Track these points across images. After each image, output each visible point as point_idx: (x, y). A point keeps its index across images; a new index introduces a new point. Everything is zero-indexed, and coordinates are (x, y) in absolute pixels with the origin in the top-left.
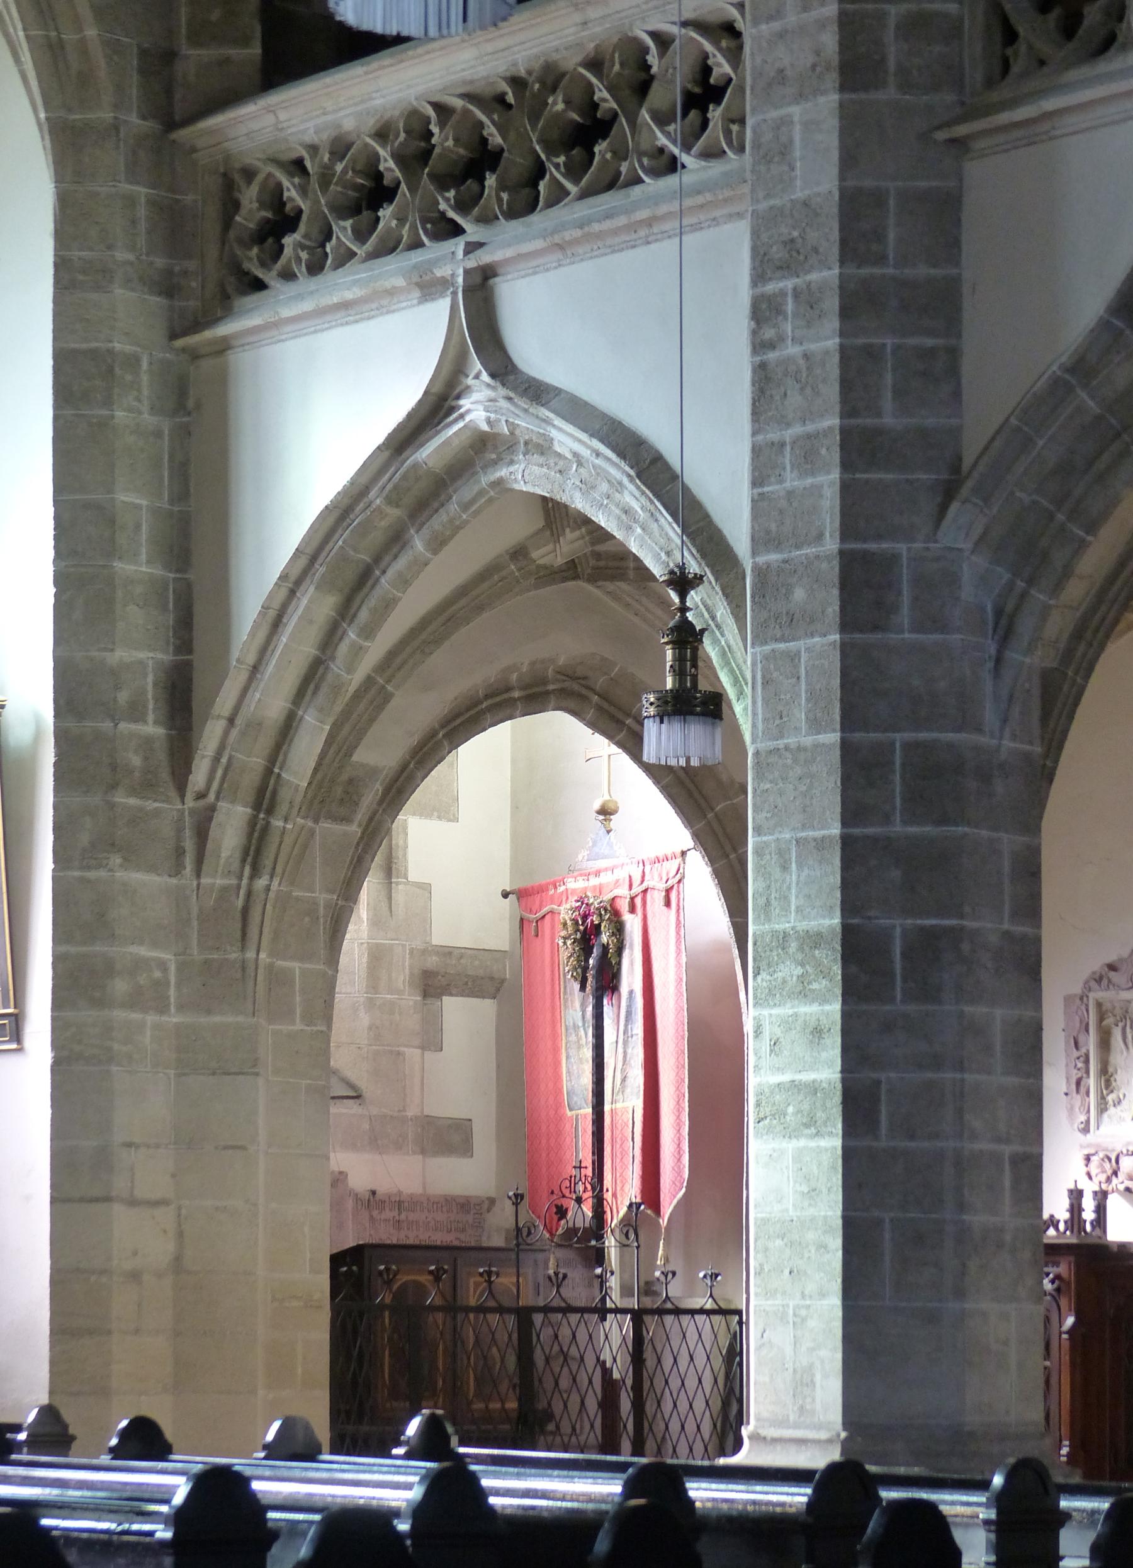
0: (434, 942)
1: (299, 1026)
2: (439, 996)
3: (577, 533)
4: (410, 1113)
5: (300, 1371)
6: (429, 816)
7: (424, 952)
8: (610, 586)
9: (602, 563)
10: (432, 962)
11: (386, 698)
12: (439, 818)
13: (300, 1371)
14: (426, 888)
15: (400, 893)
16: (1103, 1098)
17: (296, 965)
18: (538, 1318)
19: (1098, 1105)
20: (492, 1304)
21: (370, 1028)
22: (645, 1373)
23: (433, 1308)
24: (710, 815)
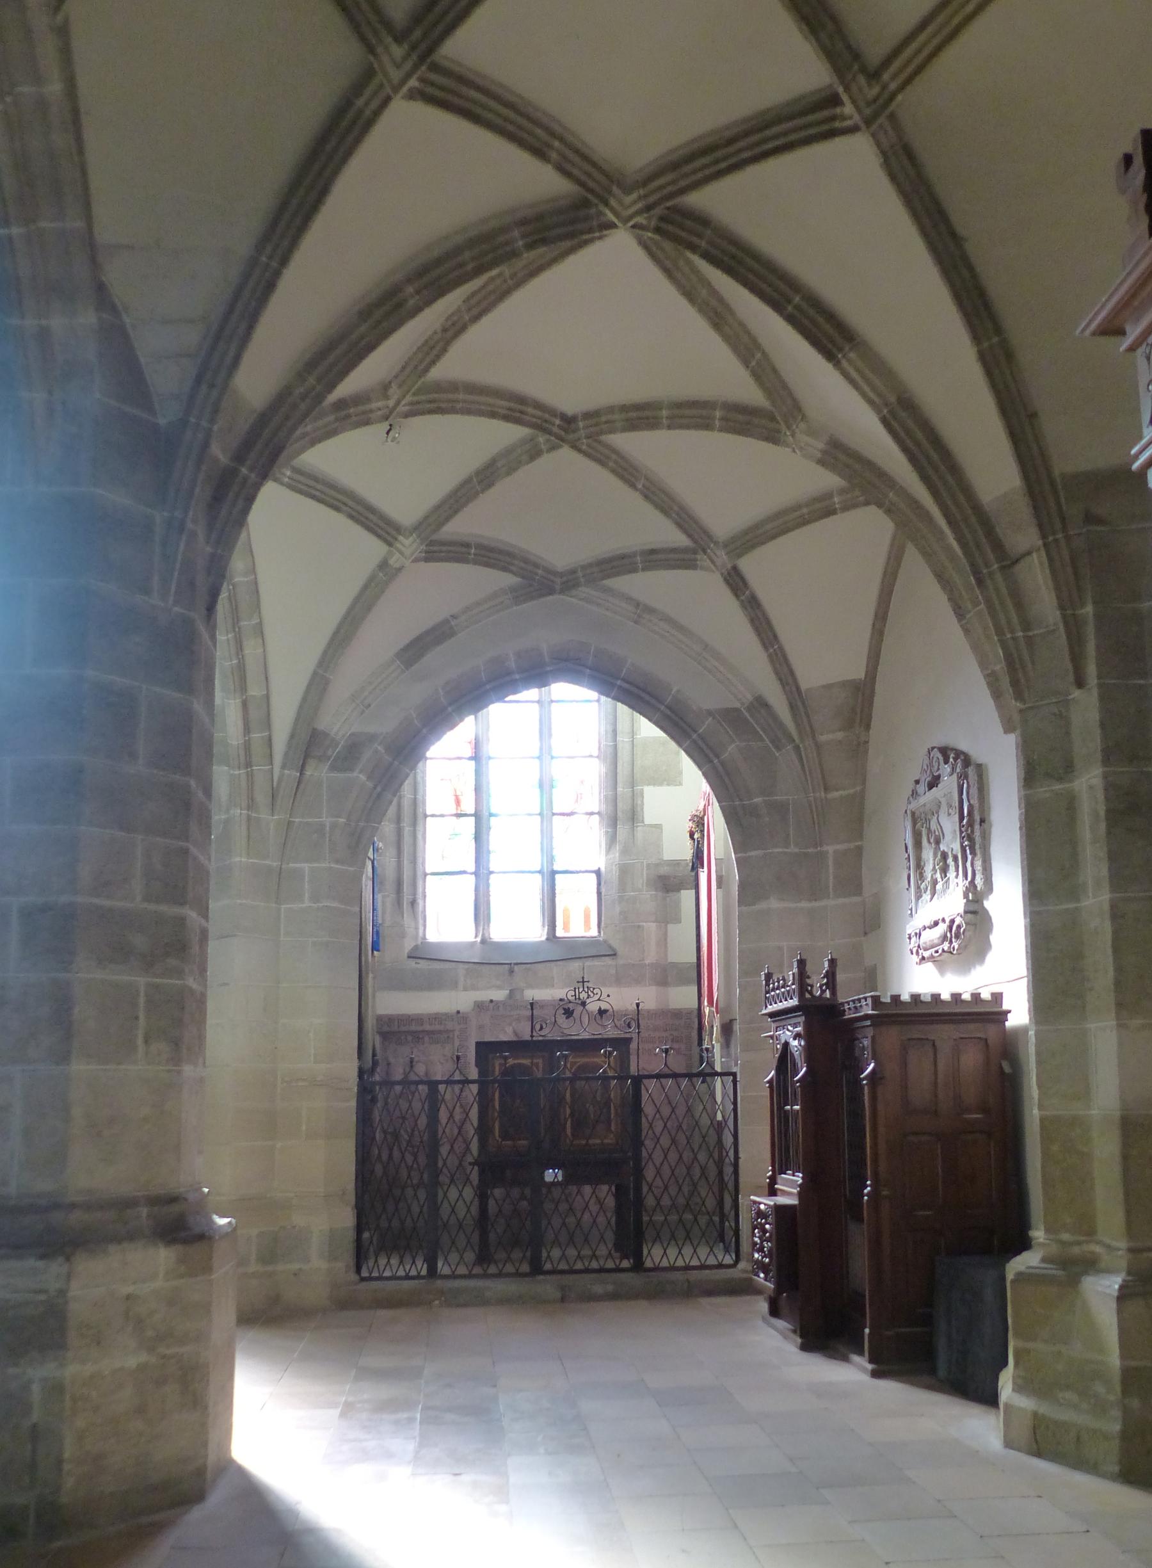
0: (665, 858)
1: (307, 904)
2: (679, 890)
3: (411, 539)
4: (647, 962)
5: (304, 1128)
6: (661, 784)
7: (657, 865)
8: (574, 592)
9: (565, 579)
10: (665, 870)
11: (327, 682)
12: (668, 785)
13: (304, 1128)
14: (658, 827)
15: (640, 832)
16: (919, 887)
17: (306, 866)
18: (442, 1087)
19: (916, 893)
20: (667, 1071)
21: (620, 913)
22: (644, 1119)
23: (614, 1078)
24: (695, 736)
